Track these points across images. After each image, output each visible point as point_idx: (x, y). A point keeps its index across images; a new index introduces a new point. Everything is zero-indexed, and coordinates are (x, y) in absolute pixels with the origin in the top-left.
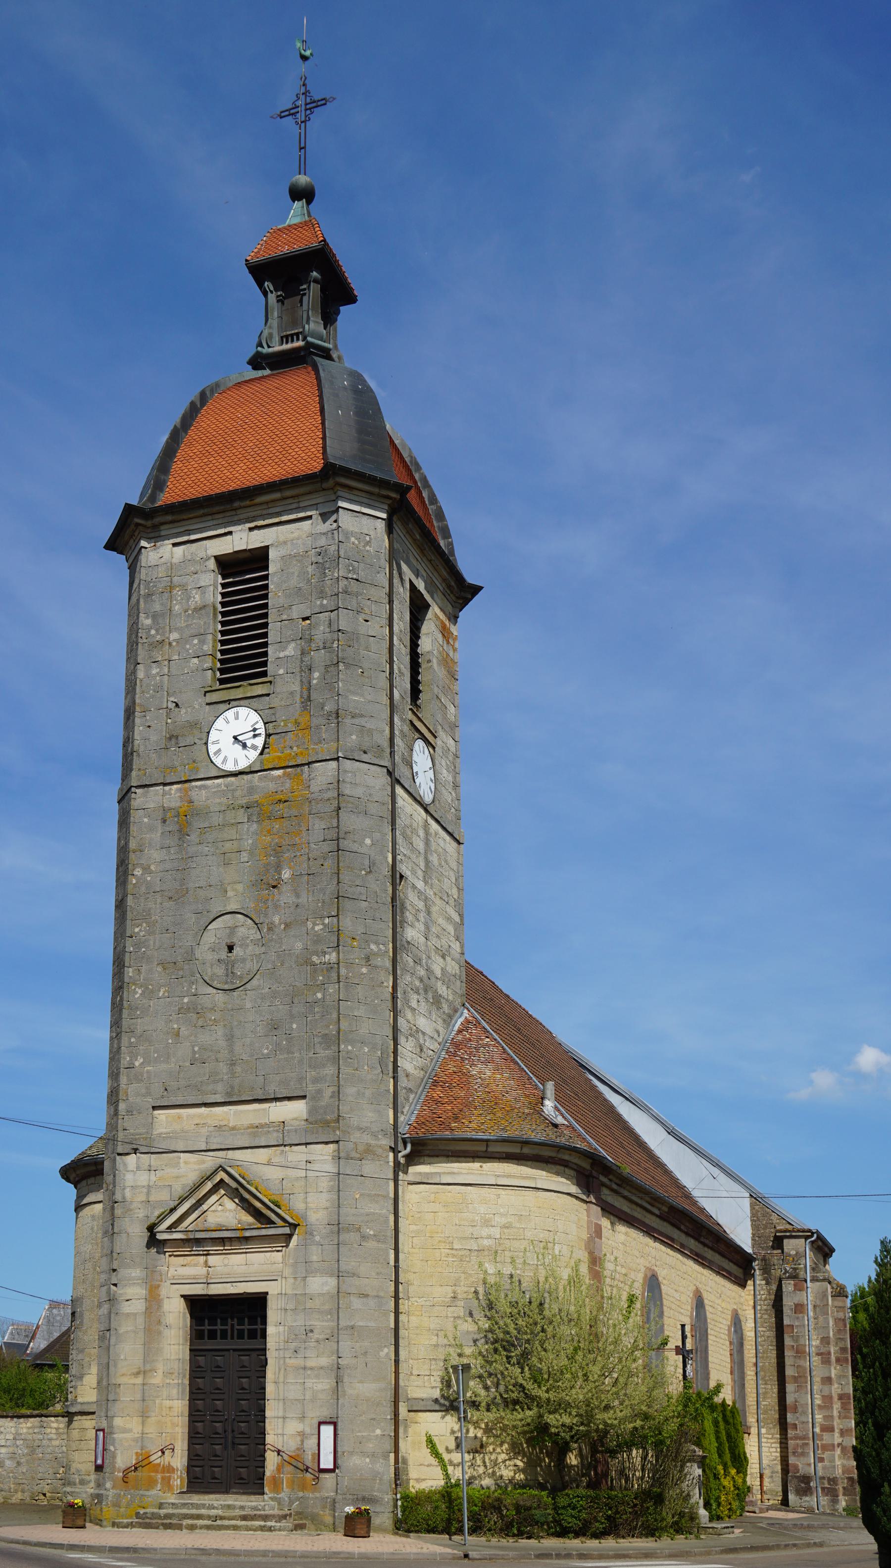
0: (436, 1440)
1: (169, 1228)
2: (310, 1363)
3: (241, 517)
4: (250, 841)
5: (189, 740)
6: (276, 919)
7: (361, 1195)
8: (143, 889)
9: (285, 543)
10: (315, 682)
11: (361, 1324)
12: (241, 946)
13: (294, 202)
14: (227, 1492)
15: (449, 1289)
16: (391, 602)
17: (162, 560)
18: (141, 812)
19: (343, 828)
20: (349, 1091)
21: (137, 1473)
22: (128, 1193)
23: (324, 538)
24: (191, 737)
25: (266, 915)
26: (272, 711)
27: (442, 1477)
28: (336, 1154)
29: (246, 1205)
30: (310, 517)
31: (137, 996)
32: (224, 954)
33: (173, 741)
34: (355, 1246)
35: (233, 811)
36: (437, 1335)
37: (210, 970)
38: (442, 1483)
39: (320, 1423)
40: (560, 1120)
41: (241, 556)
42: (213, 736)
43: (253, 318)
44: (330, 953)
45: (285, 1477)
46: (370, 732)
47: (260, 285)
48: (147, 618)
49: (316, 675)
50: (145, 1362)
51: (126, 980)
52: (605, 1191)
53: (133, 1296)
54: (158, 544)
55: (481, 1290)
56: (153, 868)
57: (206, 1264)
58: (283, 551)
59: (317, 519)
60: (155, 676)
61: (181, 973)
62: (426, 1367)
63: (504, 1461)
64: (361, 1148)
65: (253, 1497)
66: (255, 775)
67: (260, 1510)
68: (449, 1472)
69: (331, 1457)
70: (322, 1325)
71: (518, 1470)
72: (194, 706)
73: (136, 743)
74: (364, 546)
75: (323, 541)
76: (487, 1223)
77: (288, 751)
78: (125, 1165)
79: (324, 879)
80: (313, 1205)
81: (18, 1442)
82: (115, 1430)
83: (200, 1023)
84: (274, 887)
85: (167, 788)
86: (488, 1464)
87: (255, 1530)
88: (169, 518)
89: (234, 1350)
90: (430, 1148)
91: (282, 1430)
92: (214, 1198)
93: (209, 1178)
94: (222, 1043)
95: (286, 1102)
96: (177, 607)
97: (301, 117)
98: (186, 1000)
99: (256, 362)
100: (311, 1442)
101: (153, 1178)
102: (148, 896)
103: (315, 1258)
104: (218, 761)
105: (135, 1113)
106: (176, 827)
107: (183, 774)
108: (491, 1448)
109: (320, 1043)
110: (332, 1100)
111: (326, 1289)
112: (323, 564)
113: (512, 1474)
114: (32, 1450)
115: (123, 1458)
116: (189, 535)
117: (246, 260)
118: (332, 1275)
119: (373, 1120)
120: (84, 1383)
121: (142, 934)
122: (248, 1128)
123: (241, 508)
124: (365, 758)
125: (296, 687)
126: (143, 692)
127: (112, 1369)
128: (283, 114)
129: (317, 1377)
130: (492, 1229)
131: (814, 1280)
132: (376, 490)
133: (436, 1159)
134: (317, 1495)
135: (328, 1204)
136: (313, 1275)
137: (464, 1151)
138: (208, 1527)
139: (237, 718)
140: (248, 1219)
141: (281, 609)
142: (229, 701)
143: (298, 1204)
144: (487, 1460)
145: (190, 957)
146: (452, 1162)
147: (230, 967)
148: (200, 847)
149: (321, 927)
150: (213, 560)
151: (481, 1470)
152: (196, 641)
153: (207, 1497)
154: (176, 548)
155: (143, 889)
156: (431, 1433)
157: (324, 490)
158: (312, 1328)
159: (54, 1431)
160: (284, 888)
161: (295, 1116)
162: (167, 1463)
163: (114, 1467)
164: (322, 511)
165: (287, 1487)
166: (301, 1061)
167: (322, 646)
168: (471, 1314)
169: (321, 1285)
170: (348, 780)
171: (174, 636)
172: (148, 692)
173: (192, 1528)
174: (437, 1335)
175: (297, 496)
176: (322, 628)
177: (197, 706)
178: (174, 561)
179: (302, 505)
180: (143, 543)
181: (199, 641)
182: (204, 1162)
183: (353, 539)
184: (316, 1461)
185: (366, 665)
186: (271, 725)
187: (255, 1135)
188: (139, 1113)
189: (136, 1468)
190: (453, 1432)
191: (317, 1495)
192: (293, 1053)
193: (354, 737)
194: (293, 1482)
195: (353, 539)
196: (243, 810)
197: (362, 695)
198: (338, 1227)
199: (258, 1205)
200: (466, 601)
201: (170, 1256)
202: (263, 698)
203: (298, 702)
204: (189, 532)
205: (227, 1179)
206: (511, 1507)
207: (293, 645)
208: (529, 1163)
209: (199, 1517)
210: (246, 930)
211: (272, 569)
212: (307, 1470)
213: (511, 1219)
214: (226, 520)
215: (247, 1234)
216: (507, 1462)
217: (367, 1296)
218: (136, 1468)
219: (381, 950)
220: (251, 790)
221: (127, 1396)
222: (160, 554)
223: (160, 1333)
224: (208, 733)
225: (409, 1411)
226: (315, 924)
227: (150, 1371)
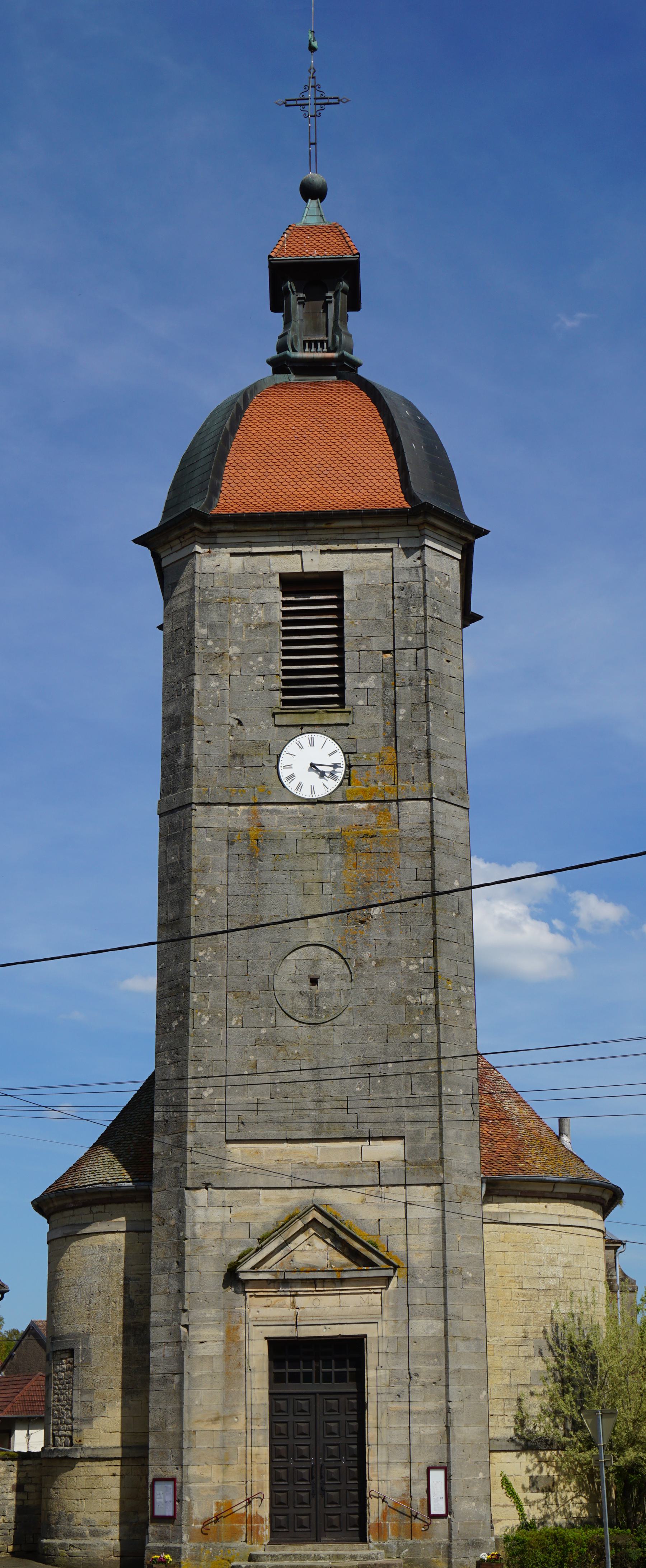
0: (511, 1480)
1: (253, 1268)
3: (312, 537)
4: (334, 874)
5: (256, 761)
6: (366, 956)
7: (462, 1237)
8: (207, 912)
9: (362, 571)
10: (401, 718)
11: (465, 1367)
12: (326, 980)
13: (307, 201)
15: (520, 1329)
17: (219, 568)
18: (203, 831)
19: (438, 870)
20: (450, 1132)
21: (218, 1524)
22: (198, 1230)
23: (407, 574)
25: (354, 950)
26: (351, 742)
27: (518, 1517)
28: (439, 1196)
29: (339, 1245)
30: (391, 550)
31: (204, 1023)
32: (306, 986)
33: (238, 760)
34: (459, 1288)
35: (313, 841)
36: (510, 1375)
37: (290, 1002)
38: (518, 1522)
39: (428, 1470)
42: (284, 760)
44: (427, 994)
48: (203, 627)
50: (225, 1406)
51: (191, 1006)
54: (214, 551)
55: (549, 1329)
56: (218, 890)
57: (293, 1305)
58: (359, 580)
59: (399, 553)
60: (214, 690)
61: (256, 1002)
62: (500, 1406)
63: (572, 1499)
64: (460, 1190)
66: (336, 805)
67: (373, 1559)
68: (525, 1512)
69: (442, 1503)
71: (584, 1507)
72: (260, 728)
73: (195, 757)
74: (445, 586)
76: (552, 1263)
77: (373, 785)
78: (194, 1200)
79: (418, 919)
80: (420, 1250)
83: (281, 1056)
84: (362, 922)
85: (232, 808)
86: (559, 1503)
88: (231, 527)
89: (321, 1394)
90: (501, 1187)
91: (385, 1478)
92: (302, 1237)
95: (382, 1142)
96: (237, 620)
97: (311, 110)
98: (263, 1031)
100: (419, 1489)
101: (228, 1215)
102: (213, 919)
103: (418, 1301)
104: (292, 786)
105: (204, 1145)
106: (246, 851)
107: (252, 796)
108: (561, 1485)
109: (419, 1084)
110: (434, 1142)
111: (431, 1332)
112: (406, 600)
113: (578, 1510)
116: (251, 547)
117: (270, 256)
118: (437, 1318)
119: (468, 1162)
120: (95, 1426)
121: (207, 958)
122: (338, 1166)
123: (313, 529)
124: (453, 799)
125: (379, 721)
126: (200, 705)
127: (186, 1415)
128: (289, 103)
129: (425, 1421)
130: (557, 1269)
132: (457, 532)
133: (504, 1199)
134: (429, 1541)
136: (417, 1317)
137: (534, 1192)
139: (312, 744)
140: (340, 1259)
141: (359, 639)
142: (302, 726)
143: (397, 1247)
144: (558, 1498)
145: (268, 985)
146: (520, 1202)
147: (314, 1002)
148: (275, 874)
149: (416, 967)
150: (277, 577)
151: (554, 1508)
152: (260, 659)
153: (302, 1547)
154: (233, 558)
156: (506, 1473)
157: (408, 525)
158: (417, 1371)
160: (374, 925)
161: (391, 1156)
163: (190, 1518)
164: (405, 546)
165: (393, 1534)
167: (408, 683)
168: (541, 1353)
170: (440, 821)
171: (234, 650)
172: (206, 706)
174: (510, 1375)
175: (378, 527)
176: (407, 665)
177: (263, 727)
178: (232, 571)
179: (381, 536)
180: (198, 548)
181: (265, 659)
182: (287, 1200)
183: (436, 578)
184: (426, 1506)
185: (449, 706)
186: (352, 756)
187: (347, 1174)
188: (210, 1146)
189: (217, 1519)
190: (528, 1471)
191: (429, 1541)
192: (389, 1092)
193: (442, 778)
194: (399, 1529)
195: (436, 578)
196: (324, 841)
197: (447, 736)
199: (357, 1246)
201: (251, 1296)
202: (341, 728)
203: (381, 735)
204: (250, 544)
205: (320, 1218)
206: (585, 1544)
207: (373, 677)
208: (583, 1203)
210: (331, 964)
212: (413, 1516)
213: (570, 1259)
214: (294, 538)
215: (346, 1275)
216: (575, 1500)
217: (468, 1339)
218: (217, 1519)
219: (468, 991)
220: (331, 821)
222: (215, 563)
224: (279, 756)
226: (409, 963)
227: (230, 1416)
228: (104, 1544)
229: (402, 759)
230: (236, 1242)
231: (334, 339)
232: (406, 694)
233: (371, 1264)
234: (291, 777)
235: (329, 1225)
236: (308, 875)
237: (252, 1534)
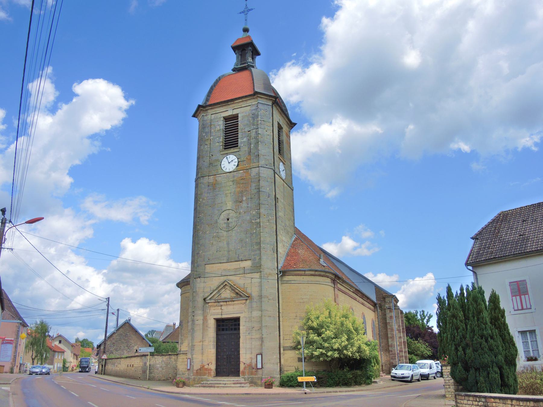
2: (253, 337)
6: (242, 211)
16: (273, 126)
22: (197, 290)
24: (215, 164)
32: (226, 221)
40: (325, 265)
43: (232, 59)
45: (246, 371)
46: (268, 160)
47: (235, 52)
52: (338, 285)
58: (242, 115)
70: (257, 326)
75: (254, 111)
94: (226, 246)
99: (234, 70)
100: (254, 361)
104: (224, 169)
115: (197, 367)
131: (395, 309)
138: (223, 387)
141: (242, 129)
143: (249, 291)
155: (202, 205)
160: (244, 202)
166: (249, 250)
169: (256, 314)
171: (212, 137)
173: (218, 387)
187: (236, 271)
198: (261, 297)
200: (292, 127)
209: (220, 384)
211: (239, 119)
221: (198, 348)
223: (207, 330)
225: (4, 366)
229: (252, 158)
232: (252, 141)
234: (224, 167)
236: (227, 192)
237: (209, 374)
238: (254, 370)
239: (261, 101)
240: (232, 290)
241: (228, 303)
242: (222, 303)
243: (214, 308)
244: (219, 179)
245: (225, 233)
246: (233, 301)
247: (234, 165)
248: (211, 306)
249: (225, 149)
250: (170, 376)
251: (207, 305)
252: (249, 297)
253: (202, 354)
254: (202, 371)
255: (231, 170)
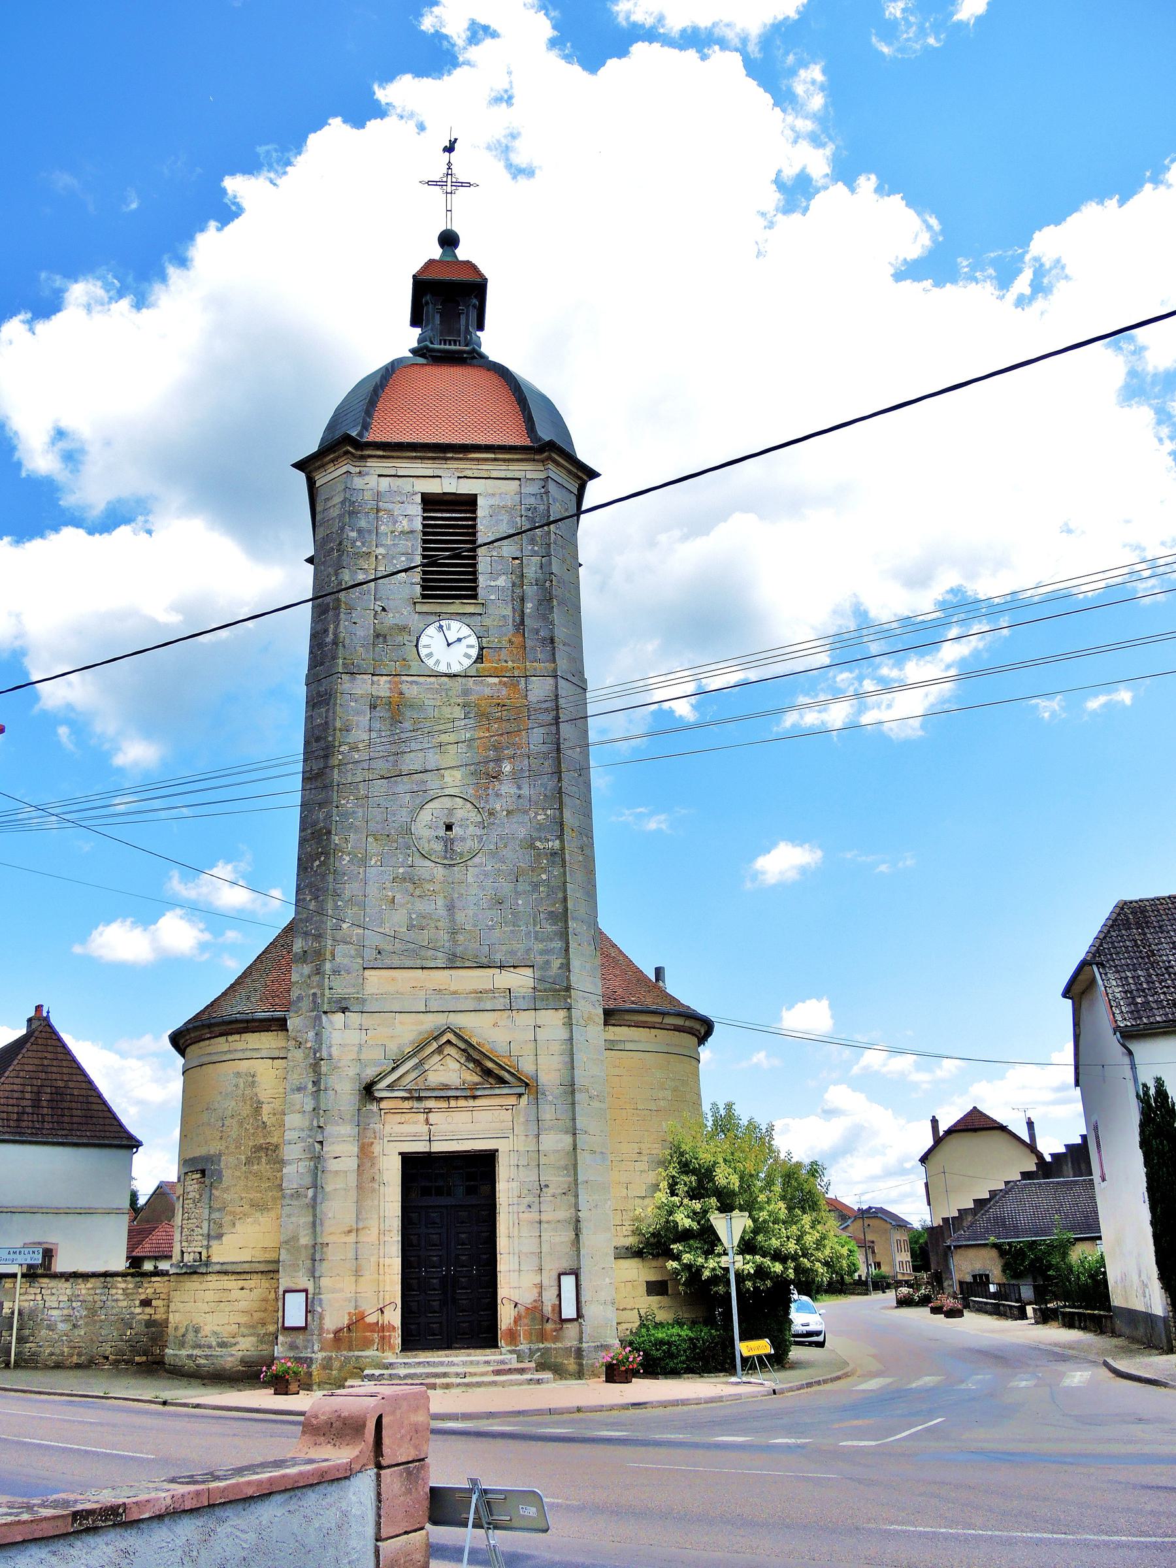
6: (498, 808)
12: (461, 826)
14: (449, 1347)
22: (335, 1051)
32: (442, 832)
33: (381, 639)
39: (559, 1275)
41: (445, 498)
45: (521, 1330)
48: (352, 530)
49: (529, 605)
53: (342, 1151)
58: (492, 501)
65: (488, 1351)
81: (74, 1304)
82: (323, 1290)
83: (417, 893)
87: (521, 1384)
93: (436, 1038)
94: (442, 912)
98: (401, 870)
100: (549, 1298)
104: (430, 662)
111: (560, 1146)
114: (92, 1312)
115: (334, 1318)
118: (566, 1132)
122: (471, 993)
123: (452, 458)
129: (555, 1229)
134: (559, 1345)
135: (560, 1066)
143: (527, 1067)
147: (449, 844)
159: (120, 1291)
162: (386, 1322)
171: (381, 550)
191: (559, 1345)
194: (531, 1334)
205: (454, 1040)
207: (504, 577)
222: (373, 478)
226: (537, 814)
228: (232, 1355)
229: (529, 643)
230: (375, 1063)
231: (466, 338)
233: (502, 1081)
234: (430, 655)
235: (463, 1046)
237: (384, 1342)
238: (549, 1326)
239: (554, 472)
240: (470, 1058)
241: (453, 1103)
242: (431, 1104)
243: (398, 1118)
244: (411, 691)
245: (440, 872)
246: (475, 1097)
247: (467, 656)
248: (390, 1112)
249: (424, 596)
250: (107, 1349)
251: (374, 1107)
252: (527, 1085)
253: (357, 1273)
254: (355, 1332)
255: (456, 668)
